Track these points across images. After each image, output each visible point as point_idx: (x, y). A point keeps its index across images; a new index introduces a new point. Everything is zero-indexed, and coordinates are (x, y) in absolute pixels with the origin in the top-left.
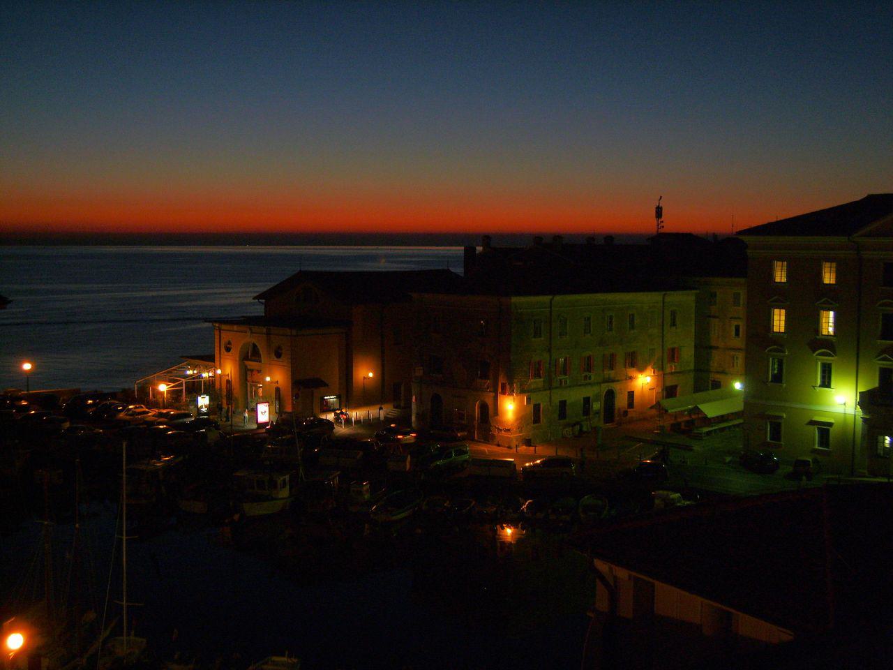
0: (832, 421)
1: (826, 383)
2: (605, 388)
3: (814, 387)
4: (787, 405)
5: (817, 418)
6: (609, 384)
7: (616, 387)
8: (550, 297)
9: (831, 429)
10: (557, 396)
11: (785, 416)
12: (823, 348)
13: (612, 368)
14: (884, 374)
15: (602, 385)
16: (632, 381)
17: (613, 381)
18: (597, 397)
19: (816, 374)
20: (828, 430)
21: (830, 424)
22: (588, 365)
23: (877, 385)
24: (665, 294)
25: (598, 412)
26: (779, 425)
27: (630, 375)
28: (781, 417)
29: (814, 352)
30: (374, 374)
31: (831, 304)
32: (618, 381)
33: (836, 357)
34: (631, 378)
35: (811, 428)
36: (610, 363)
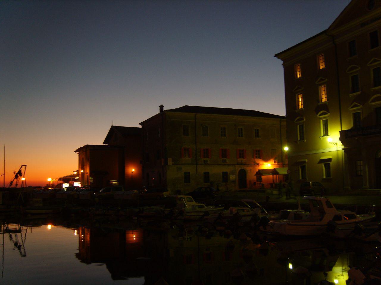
0: (330, 157)
1: (326, 134)
2: (238, 168)
3: (319, 137)
4: (308, 153)
5: (322, 158)
6: (242, 166)
7: (248, 168)
8: (195, 114)
9: (331, 163)
10: (202, 170)
11: (307, 160)
12: (323, 110)
13: (243, 157)
14: (356, 117)
15: (236, 166)
16: (259, 166)
17: (245, 164)
18: (233, 173)
19: (320, 128)
20: (329, 164)
21: (330, 160)
22: (224, 154)
23: (352, 126)
24: (281, 120)
25: (234, 181)
26: (304, 166)
27: (257, 162)
28: (305, 162)
29: (317, 114)
30: (134, 168)
31: (325, 80)
32: (248, 165)
33: (329, 114)
34: (258, 164)
35: (320, 164)
36: (242, 154)
